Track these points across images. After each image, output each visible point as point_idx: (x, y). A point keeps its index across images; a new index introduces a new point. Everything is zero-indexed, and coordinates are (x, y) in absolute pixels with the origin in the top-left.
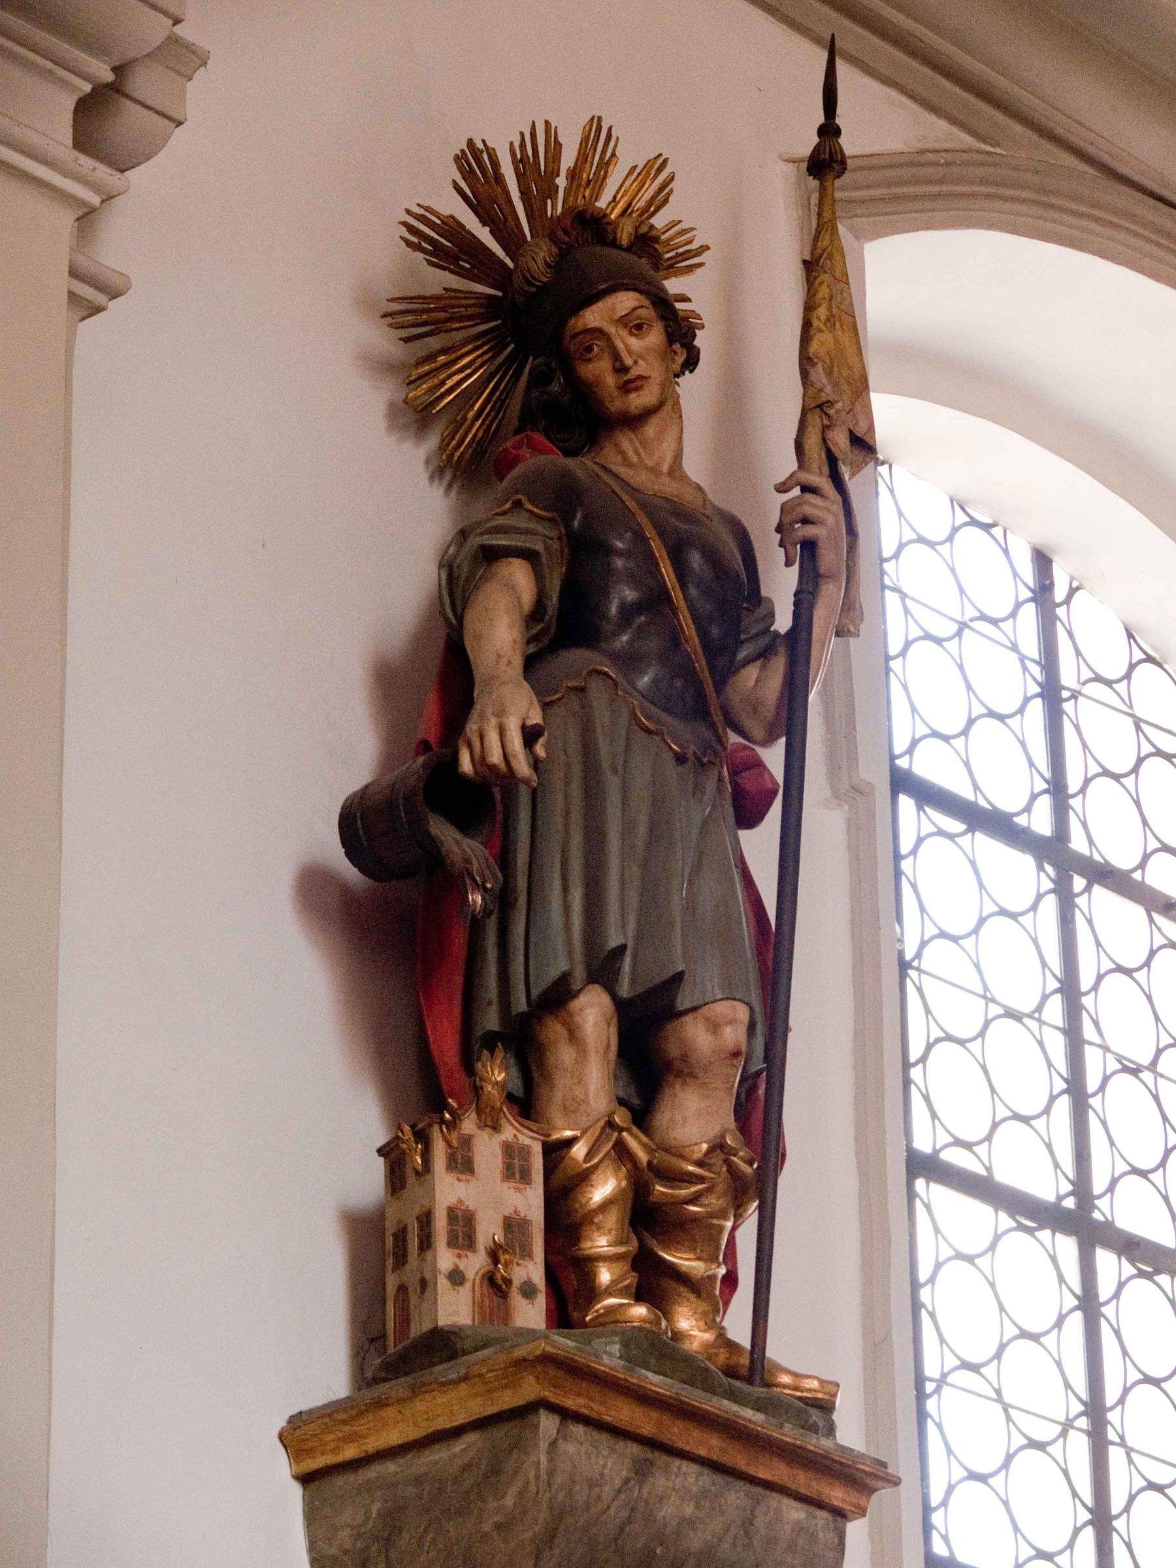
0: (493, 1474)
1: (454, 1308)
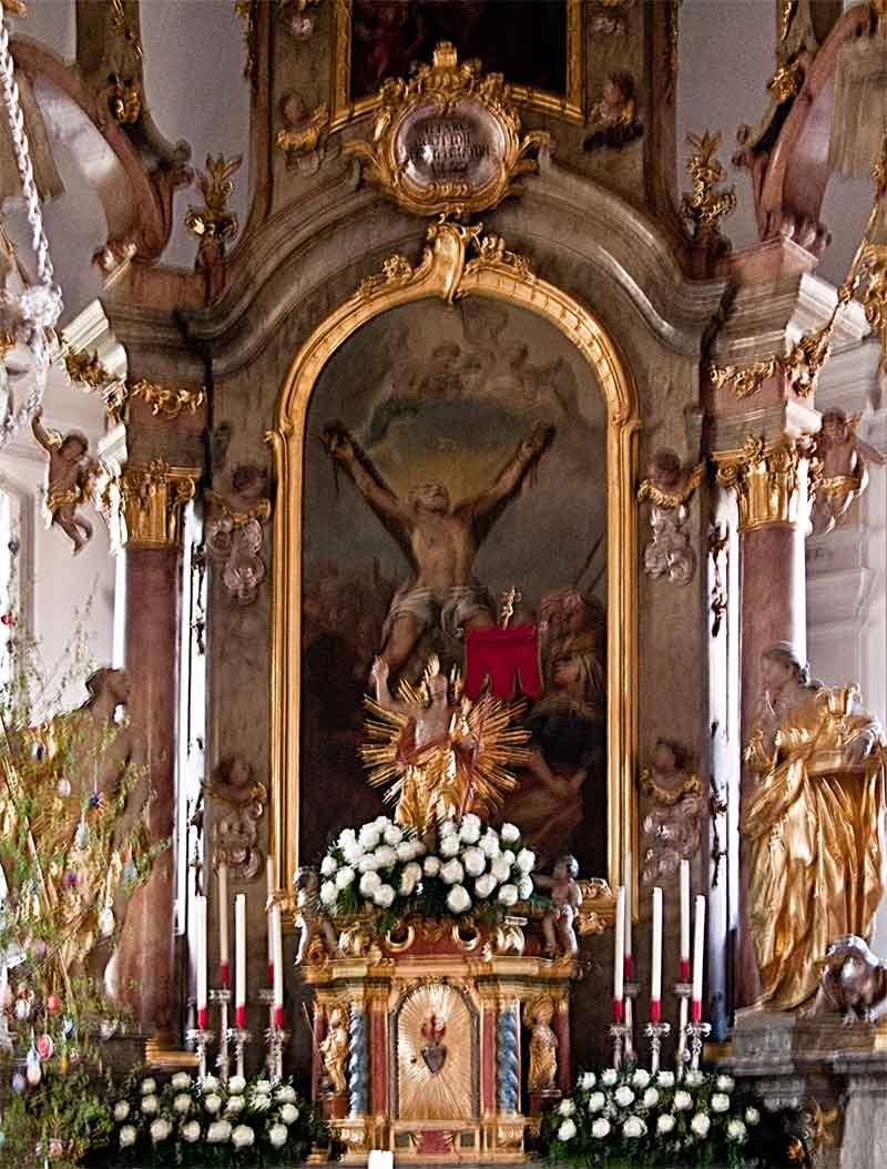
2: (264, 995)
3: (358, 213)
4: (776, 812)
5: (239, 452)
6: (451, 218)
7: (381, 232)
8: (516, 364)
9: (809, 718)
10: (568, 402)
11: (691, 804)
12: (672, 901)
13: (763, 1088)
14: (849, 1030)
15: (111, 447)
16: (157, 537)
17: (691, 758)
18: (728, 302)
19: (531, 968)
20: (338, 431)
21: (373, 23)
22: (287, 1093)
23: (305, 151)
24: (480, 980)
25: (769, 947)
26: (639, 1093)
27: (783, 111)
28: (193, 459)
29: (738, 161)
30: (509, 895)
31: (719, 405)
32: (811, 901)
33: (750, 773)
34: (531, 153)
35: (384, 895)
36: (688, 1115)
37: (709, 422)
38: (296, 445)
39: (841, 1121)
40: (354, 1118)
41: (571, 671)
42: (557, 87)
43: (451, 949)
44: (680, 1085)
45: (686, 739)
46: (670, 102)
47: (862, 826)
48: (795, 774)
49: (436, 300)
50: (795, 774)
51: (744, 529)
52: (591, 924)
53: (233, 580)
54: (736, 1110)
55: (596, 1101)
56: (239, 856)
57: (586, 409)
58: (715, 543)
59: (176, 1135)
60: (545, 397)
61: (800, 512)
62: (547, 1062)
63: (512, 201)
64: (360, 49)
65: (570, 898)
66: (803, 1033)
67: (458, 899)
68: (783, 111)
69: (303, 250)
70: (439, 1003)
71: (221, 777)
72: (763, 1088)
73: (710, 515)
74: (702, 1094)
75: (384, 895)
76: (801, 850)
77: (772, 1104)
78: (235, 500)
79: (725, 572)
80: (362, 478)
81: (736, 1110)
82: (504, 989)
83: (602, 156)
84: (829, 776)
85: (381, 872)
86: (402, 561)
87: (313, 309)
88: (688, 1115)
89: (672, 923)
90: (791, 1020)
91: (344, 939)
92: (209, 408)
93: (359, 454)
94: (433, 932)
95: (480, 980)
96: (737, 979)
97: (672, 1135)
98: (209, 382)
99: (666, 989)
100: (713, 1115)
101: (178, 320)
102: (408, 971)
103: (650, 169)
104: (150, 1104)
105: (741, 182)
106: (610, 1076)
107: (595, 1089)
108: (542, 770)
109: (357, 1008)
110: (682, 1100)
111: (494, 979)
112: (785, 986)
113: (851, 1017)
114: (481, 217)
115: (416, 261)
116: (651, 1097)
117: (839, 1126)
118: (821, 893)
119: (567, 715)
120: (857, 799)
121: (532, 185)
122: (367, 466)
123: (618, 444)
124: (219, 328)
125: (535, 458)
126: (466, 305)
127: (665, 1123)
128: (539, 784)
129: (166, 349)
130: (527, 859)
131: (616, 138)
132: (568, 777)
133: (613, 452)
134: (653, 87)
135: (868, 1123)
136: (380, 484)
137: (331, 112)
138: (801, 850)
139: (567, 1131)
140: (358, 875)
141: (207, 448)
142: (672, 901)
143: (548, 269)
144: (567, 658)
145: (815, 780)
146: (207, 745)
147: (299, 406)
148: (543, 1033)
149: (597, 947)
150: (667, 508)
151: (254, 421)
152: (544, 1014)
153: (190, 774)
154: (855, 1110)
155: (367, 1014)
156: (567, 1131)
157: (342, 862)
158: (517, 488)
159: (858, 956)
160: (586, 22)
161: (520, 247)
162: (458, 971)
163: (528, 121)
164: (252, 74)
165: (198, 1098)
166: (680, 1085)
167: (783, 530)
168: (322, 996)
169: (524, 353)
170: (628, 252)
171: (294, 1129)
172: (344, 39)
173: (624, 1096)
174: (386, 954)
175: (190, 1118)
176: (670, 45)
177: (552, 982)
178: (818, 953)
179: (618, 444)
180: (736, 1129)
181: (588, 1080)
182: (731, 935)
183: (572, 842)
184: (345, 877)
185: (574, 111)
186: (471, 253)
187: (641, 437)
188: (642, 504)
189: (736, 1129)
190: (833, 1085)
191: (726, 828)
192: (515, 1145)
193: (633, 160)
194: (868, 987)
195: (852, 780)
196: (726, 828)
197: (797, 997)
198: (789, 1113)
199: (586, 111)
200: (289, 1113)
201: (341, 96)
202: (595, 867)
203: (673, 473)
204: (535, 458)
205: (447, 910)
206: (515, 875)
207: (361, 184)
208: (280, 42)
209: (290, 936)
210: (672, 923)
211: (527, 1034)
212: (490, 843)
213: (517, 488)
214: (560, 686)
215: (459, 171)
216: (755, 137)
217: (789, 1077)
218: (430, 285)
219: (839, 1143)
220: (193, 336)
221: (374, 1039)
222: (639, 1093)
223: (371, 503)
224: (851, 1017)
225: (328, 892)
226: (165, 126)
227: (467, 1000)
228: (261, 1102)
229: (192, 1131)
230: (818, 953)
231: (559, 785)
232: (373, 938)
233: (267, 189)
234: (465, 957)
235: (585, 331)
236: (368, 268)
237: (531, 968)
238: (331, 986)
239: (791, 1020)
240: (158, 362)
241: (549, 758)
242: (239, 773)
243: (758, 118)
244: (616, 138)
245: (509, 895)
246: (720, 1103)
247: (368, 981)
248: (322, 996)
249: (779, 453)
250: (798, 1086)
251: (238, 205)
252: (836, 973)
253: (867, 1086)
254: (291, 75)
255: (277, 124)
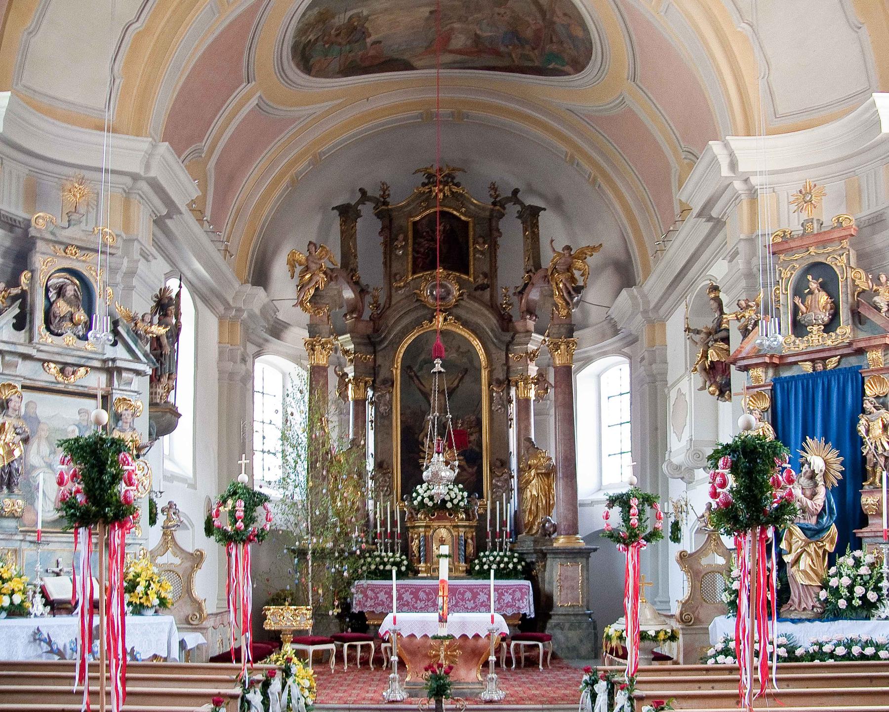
0: (163, 416)
1: (158, 401)
2: (395, 529)
3: (416, 308)
4: (528, 482)
5: (383, 374)
6: (440, 310)
7: (421, 313)
8: (457, 351)
9: (536, 457)
10: (471, 361)
11: (505, 476)
12: (501, 504)
13: (525, 556)
14: (547, 540)
15: (350, 371)
16: (361, 396)
17: (504, 463)
18: (513, 338)
19: (467, 523)
20: (410, 367)
21: (418, 252)
22: (404, 557)
23: (400, 288)
24: (454, 527)
25: (527, 518)
26: (495, 557)
27: (526, 285)
28: (372, 375)
29: (514, 294)
30: (462, 504)
31: (511, 364)
32: (537, 506)
33: (520, 470)
34: (461, 295)
35: (430, 504)
36: (508, 563)
37: (508, 368)
38: (399, 371)
39: (545, 565)
40: (422, 564)
41: (473, 438)
42: (467, 273)
43: (447, 518)
44: (505, 556)
45: (503, 458)
46: (496, 276)
47: (550, 486)
48: (533, 472)
49: (435, 331)
50: (533, 472)
51: (517, 398)
52: (481, 511)
53: (382, 409)
54: (519, 562)
55: (484, 560)
56: (383, 489)
57: (476, 364)
58: (510, 402)
59: (377, 568)
60: (465, 360)
61: (532, 394)
62: (471, 549)
63: (456, 306)
64: (415, 260)
65: (476, 504)
66: (536, 542)
67: (449, 505)
68: (526, 285)
69: (401, 317)
70: (443, 532)
71: (380, 465)
72: (525, 556)
73: (509, 394)
74: (511, 558)
75: (430, 504)
76: (534, 493)
77: (528, 560)
78: (383, 387)
79: (513, 408)
80: (417, 381)
81: (519, 562)
82: (461, 529)
83: (479, 292)
84: (542, 474)
85: (429, 497)
86: (427, 405)
87: (403, 333)
88: (508, 563)
89: (501, 509)
90: (532, 538)
91: (419, 516)
92: (375, 360)
93: (416, 375)
94: (441, 513)
95: (454, 527)
96: (518, 528)
97: (504, 569)
98: (375, 353)
99: (500, 528)
100: (514, 563)
101: (369, 337)
102: (436, 524)
103: (492, 296)
104: (369, 560)
105: (515, 299)
106: (487, 553)
107: (484, 557)
108: (466, 467)
109: (422, 534)
110: (506, 559)
111: (457, 527)
112: (531, 529)
113: (547, 537)
114: (447, 311)
115: (431, 322)
116: (498, 559)
117: (545, 566)
118: (540, 504)
119: (472, 450)
120: (548, 479)
121: (461, 302)
122: (417, 377)
123: (484, 374)
124: (378, 340)
125: (463, 377)
126: (443, 333)
127: (502, 566)
128: (465, 470)
129: (365, 344)
130: (466, 494)
131: (482, 288)
132: (473, 468)
133: (483, 377)
134: (492, 274)
135: (552, 565)
136: (422, 384)
137: (407, 277)
138: (534, 493)
139: (477, 568)
140: (423, 498)
141: (374, 371)
142: (501, 504)
143: (466, 324)
144: (471, 434)
145: (538, 474)
146: (376, 456)
147: (400, 360)
148: (470, 541)
149: (483, 517)
150: (497, 393)
151: (387, 364)
152: (470, 536)
153: (370, 465)
154: (549, 562)
155: (425, 536)
156: (477, 568)
157: (418, 494)
158: (458, 386)
159: (549, 521)
160: (474, 255)
161: (458, 318)
162: (448, 524)
163: (462, 284)
164: (385, 263)
165: (382, 558)
166: (505, 556)
167: (527, 400)
168: (411, 530)
169: (459, 347)
170: (488, 321)
171: (407, 566)
172: (410, 256)
173: (491, 558)
174: (430, 520)
175: (380, 564)
176: (496, 261)
177: (470, 527)
178: (539, 520)
179: (484, 374)
180: (519, 567)
181: (482, 554)
182: (516, 512)
183: (473, 486)
184: (419, 498)
185: (471, 279)
186: (445, 320)
187: (491, 373)
188: (491, 391)
189: (519, 567)
190: (543, 555)
191: (514, 482)
192: (463, 571)
193: (487, 294)
194: (552, 529)
195: (547, 475)
196: (514, 482)
197: (534, 531)
198: (532, 563)
199: (474, 280)
200: (405, 562)
201: (410, 274)
202: (481, 497)
203: (499, 383)
204: (463, 377)
205: (446, 508)
206: (463, 498)
207: (417, 300)
208: (393, 257)
209: (403, 513)
210: (501, 509)
211: (466, 541)
212: (456, 490)
213: (458, 386)
214: (470, 442)
215: (443, 299)
216: (519, 289)
217: (532, 553)
218: (435, 327)
219: (545, 571)
220: (372, 340)
221: (427, 542)
222: (495, 557)
223: (420, 390)
224: (547, 537)
225: (415, 503)
226: (363, 282)
227: (451, 532)
228: (398, 559)
229: (381, 567)
230: (539, 520)
231: (470, 470)
232: (426, 516)
233: (390, 297)
234: (451, 520)
235: (477, 344)
236: (418, 323)
237: (467, 523)
238: (414, 527)
239: (532, 538)
240: (362, 348)
241: (467, 462)
242: (385, 466)
243: (520, 283)
244: (482, 288)
245: (462, 504)
246: (515, 560)
247: (426, 527)
248: (411, 530)
249: (526, 380)
250: (535, 555)
251: (382, 301)
252: (544, 525)
253: (552, 556)
254: (396, 267)
255: (393, 280)
